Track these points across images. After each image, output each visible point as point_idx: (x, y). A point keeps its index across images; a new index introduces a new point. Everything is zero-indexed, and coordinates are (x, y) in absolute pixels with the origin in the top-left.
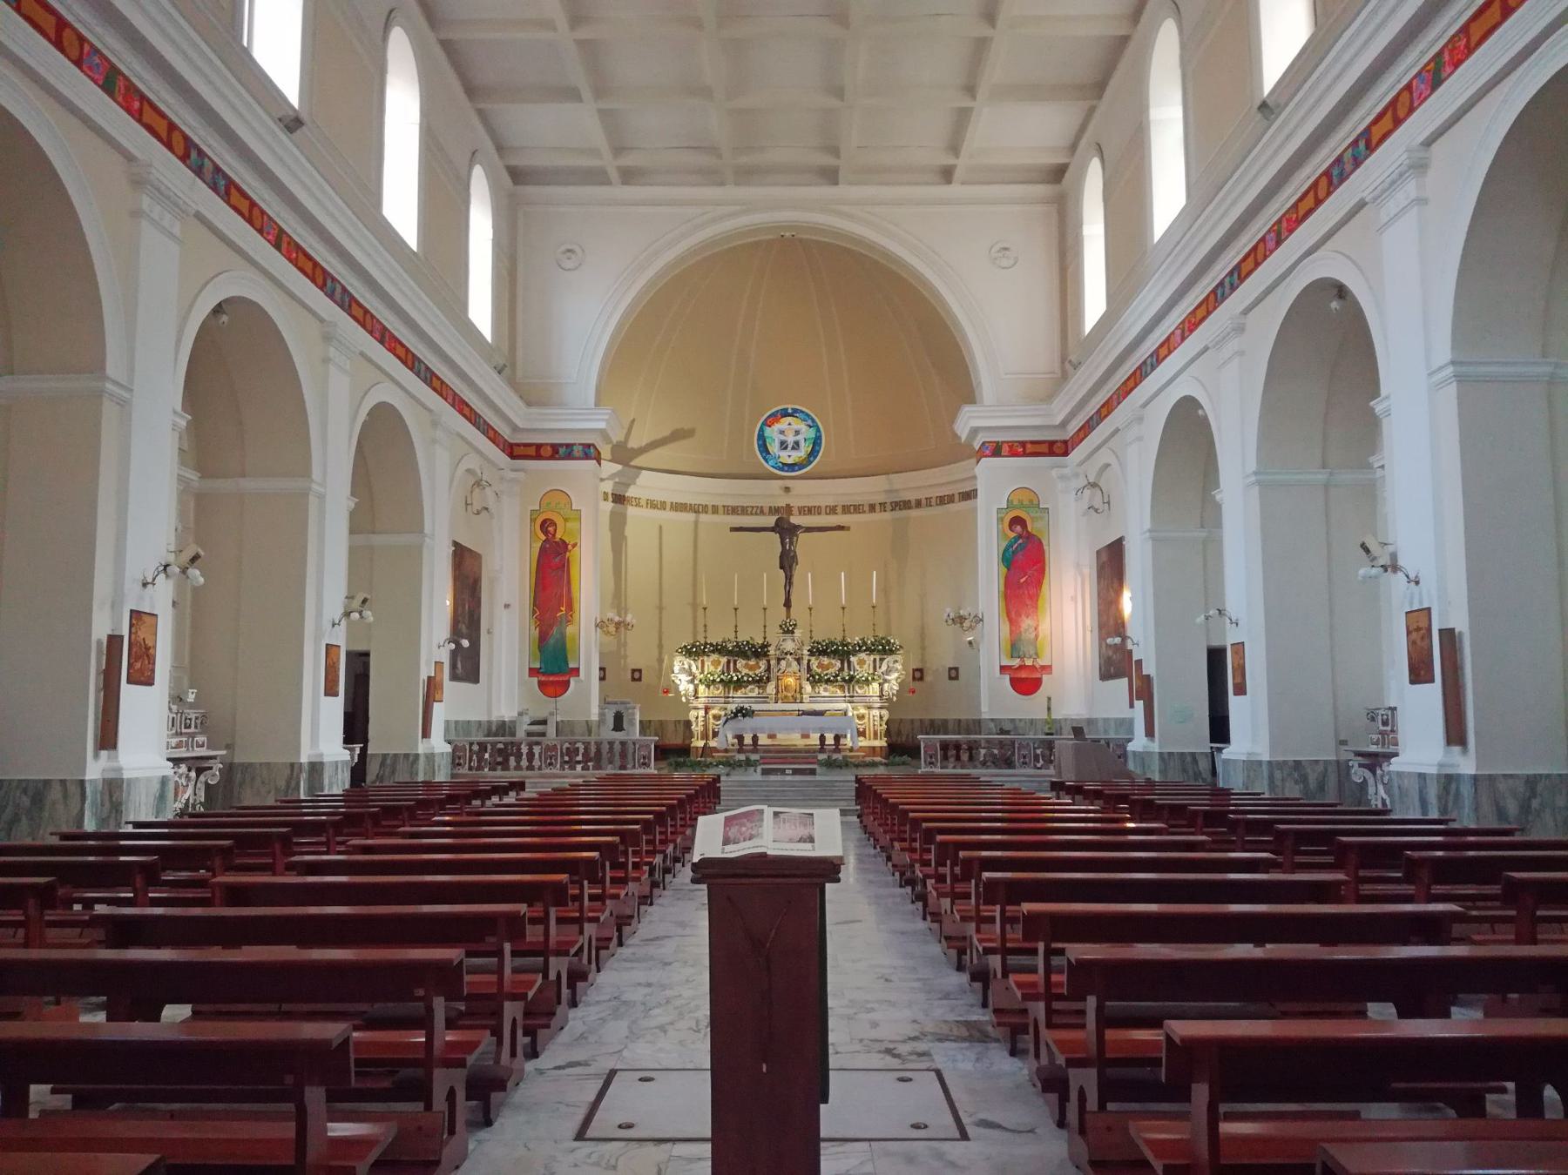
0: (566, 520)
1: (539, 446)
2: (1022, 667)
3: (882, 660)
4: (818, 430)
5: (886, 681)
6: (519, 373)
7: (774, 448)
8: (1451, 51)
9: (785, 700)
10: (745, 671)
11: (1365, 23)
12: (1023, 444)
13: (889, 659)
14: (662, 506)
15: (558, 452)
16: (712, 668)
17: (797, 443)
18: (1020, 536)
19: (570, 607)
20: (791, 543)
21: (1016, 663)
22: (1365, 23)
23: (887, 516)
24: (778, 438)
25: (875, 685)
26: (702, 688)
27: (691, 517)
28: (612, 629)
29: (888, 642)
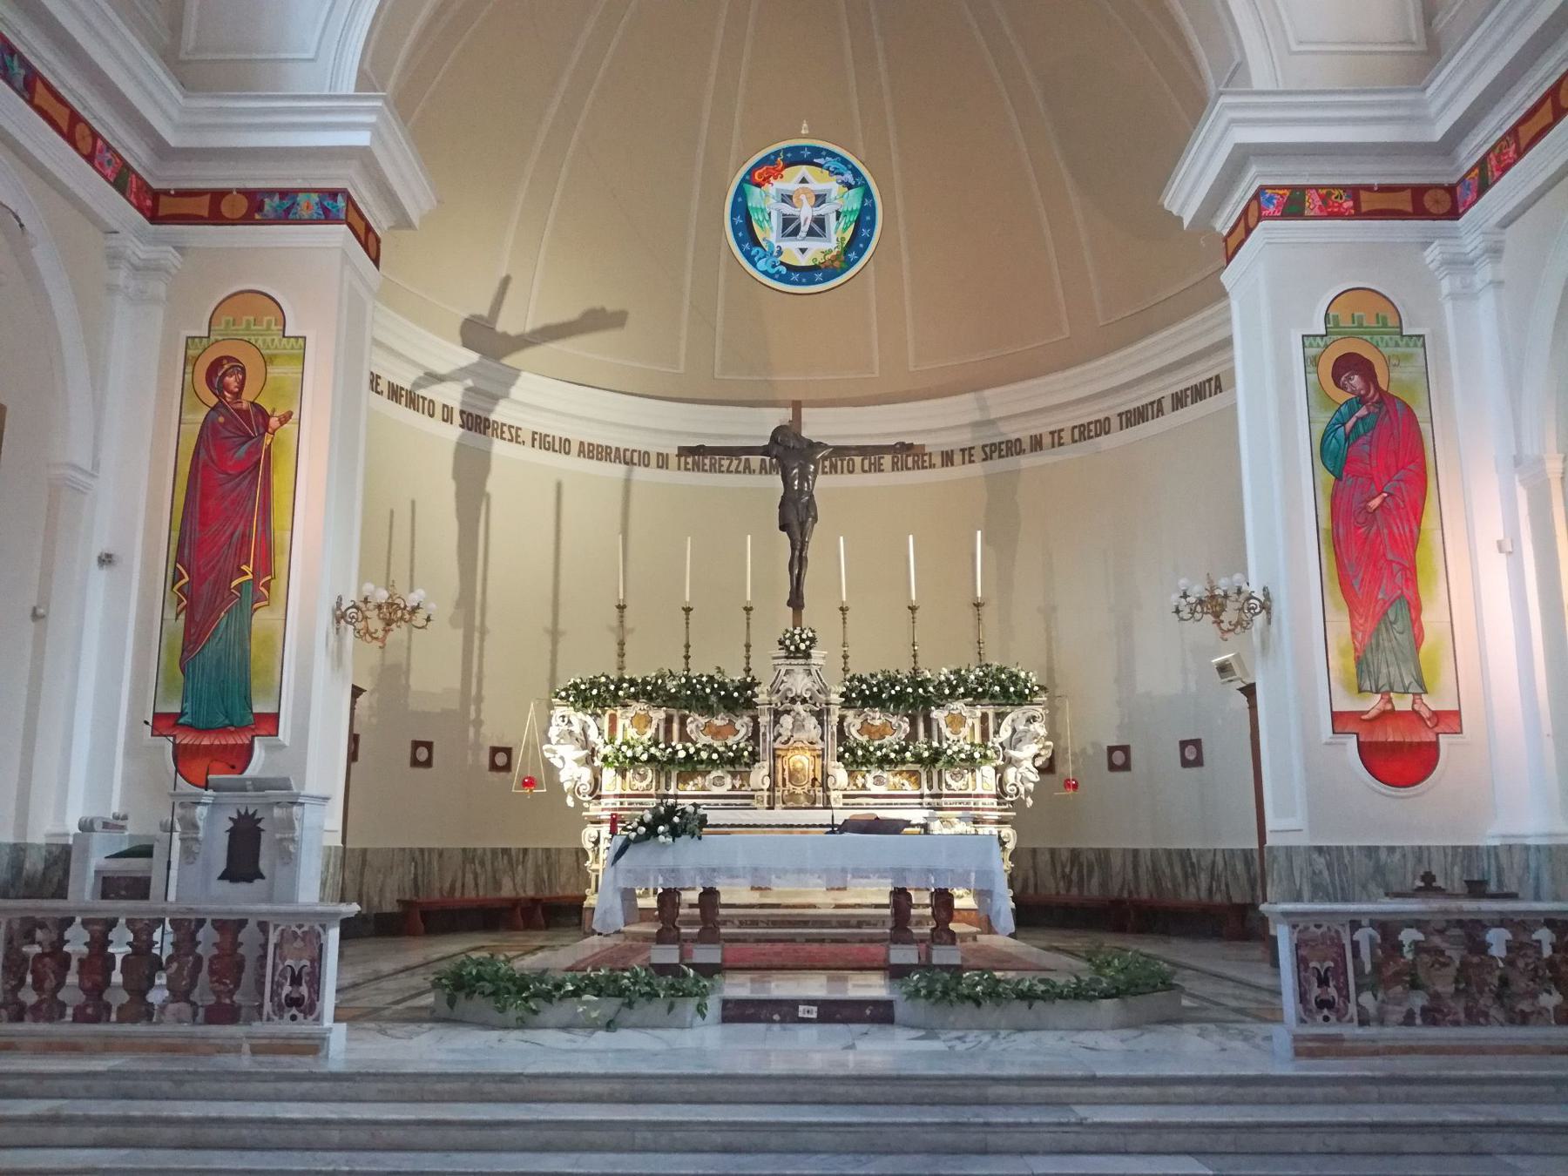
0: (267, 361)
1: (218, 196)
2: (1387, 715)
3: (1000, 716)
4: (868, 194)
5: (1009, 762)
6: (190, 37)
7: (768, 232)
8: (1497, 157)
9: (791, 802)
10: (704, 739)
11: (1467, 57)
12: (1354, 191)
13: (1016, 715)
14: (564, 446)
15: (258, 207)
16: (632, 733)
17: (820, 222)
18: (1362, 400)
19: (265, 565)
20: (803, 477)
21: (1372, 704)
22: (1467, 57)
23: (977, 469)
24: (777, 209)
25: (988, 771)
26: (609, 775)
27: (619, 470)
28: (376, 624)
29: (1014, 679)
